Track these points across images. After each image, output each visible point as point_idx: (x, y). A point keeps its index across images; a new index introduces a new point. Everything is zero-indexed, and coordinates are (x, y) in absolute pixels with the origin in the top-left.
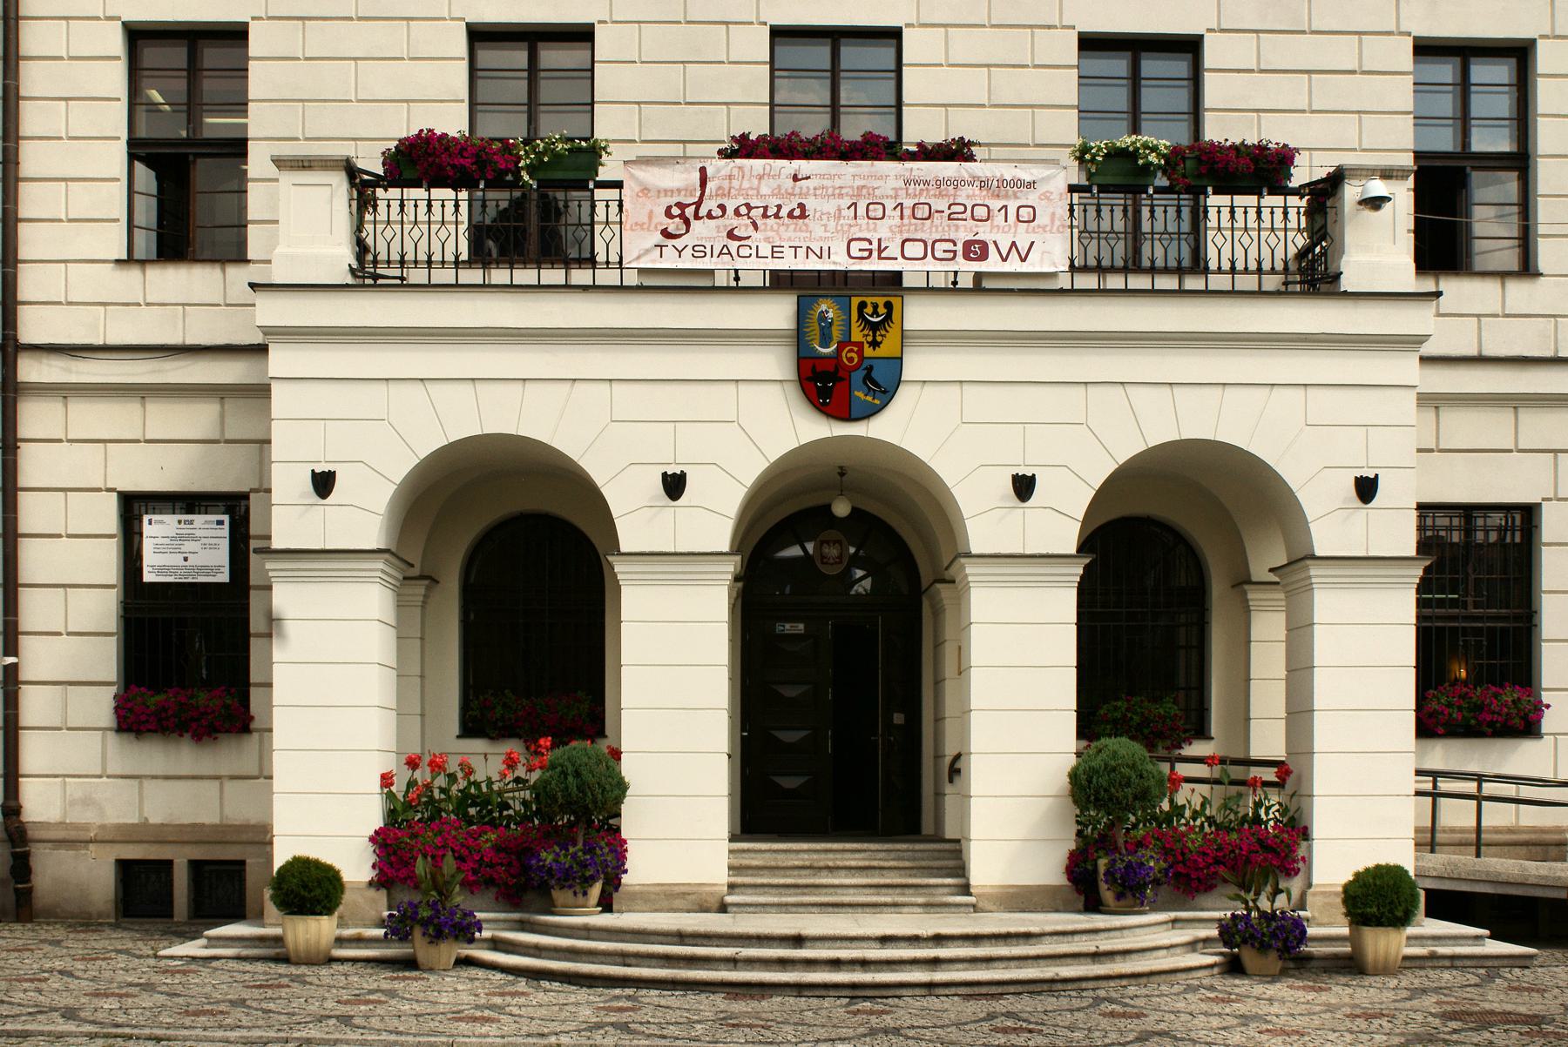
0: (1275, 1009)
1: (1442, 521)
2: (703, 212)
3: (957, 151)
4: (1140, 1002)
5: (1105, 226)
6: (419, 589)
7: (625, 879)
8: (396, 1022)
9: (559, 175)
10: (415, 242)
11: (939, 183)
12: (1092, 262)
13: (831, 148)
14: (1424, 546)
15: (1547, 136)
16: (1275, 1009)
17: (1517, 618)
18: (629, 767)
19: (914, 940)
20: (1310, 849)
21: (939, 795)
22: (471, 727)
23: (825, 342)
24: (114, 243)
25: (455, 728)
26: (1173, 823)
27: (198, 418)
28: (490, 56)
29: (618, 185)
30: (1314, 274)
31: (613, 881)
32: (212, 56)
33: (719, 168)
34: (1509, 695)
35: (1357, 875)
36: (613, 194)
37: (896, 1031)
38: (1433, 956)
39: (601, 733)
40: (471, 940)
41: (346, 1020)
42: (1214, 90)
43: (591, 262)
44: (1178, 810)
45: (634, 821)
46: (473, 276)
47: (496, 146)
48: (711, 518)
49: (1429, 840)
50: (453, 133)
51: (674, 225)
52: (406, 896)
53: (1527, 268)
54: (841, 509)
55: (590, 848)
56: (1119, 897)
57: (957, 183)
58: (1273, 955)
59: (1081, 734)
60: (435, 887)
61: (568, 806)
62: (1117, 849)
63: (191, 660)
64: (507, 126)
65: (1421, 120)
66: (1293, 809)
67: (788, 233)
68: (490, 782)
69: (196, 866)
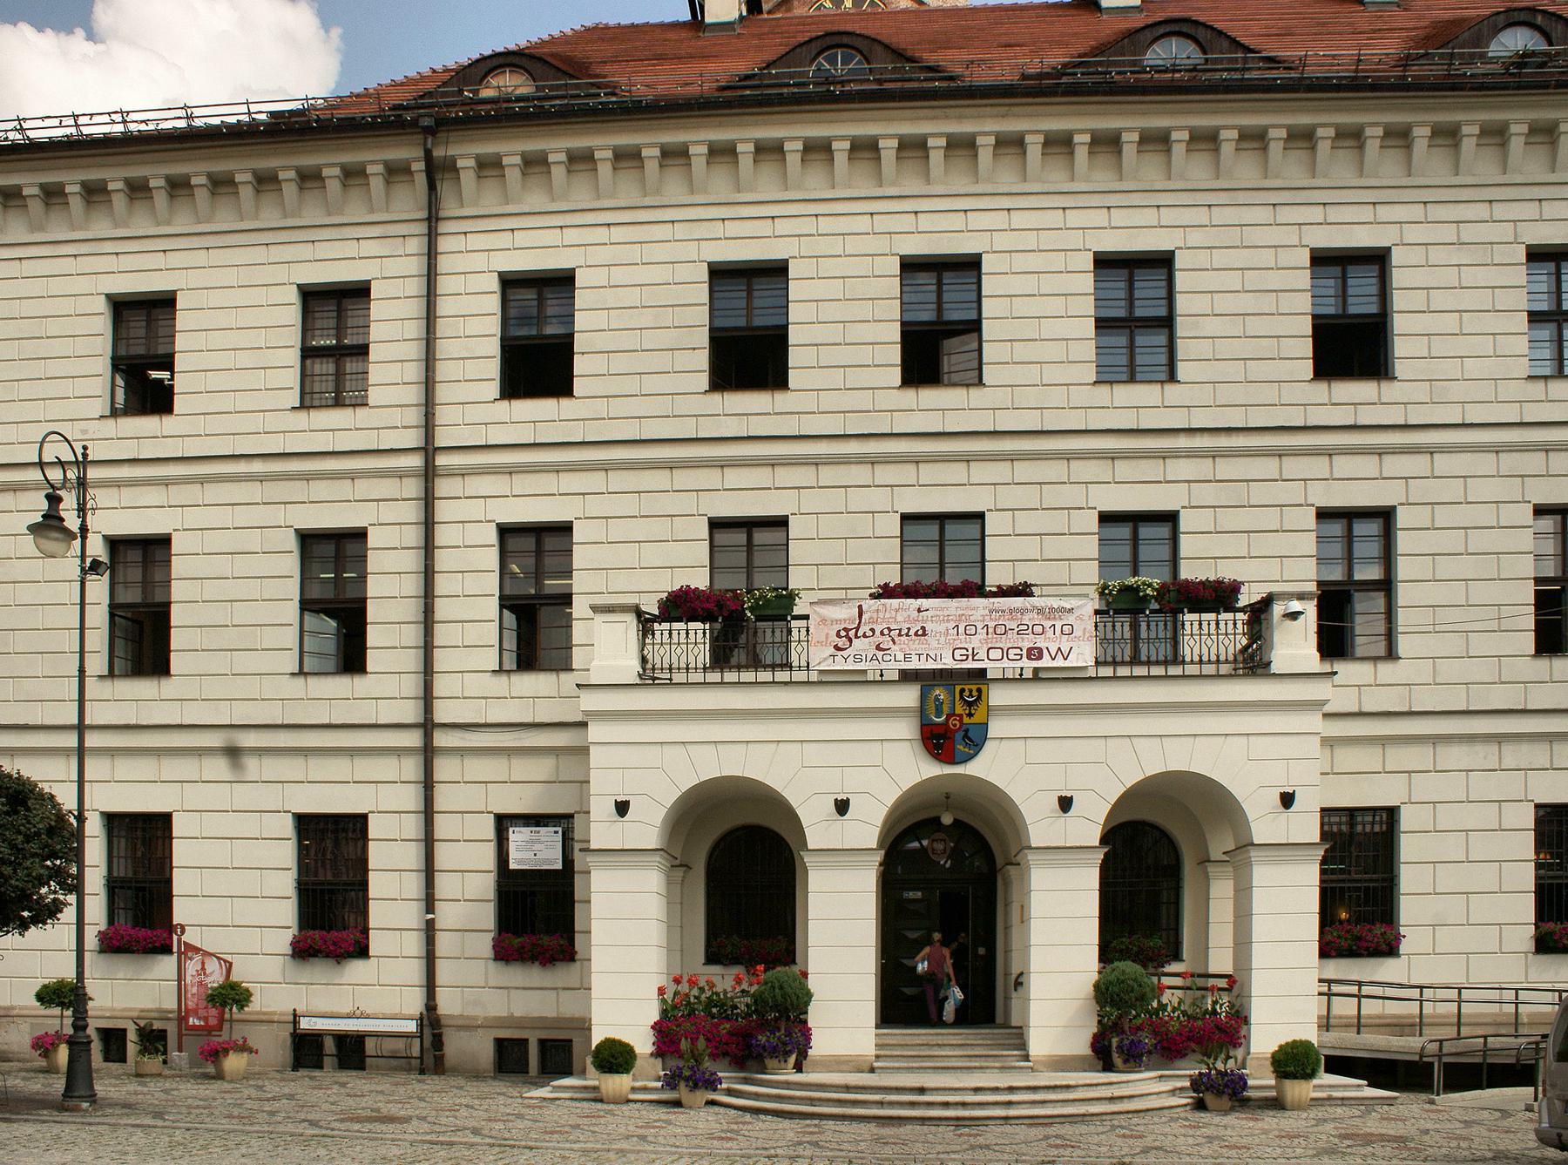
0: (1229, 1132)
1: (1335, 819)
2: (860, 633)
3: (1023, 590)
4: (1141, 1128)
5: (1118, 635)
6: (679, 873)
7: (810, 1052)
8: (673, 1140)
9: (769, 612)
10: (678, 656)
11: (1011, 611)
12: (1110, 659)
13: (942, 591)
14: (1325, 836)
15: (1405, 568)
16: (1229, 1132)
17: (1384, 880)
18: (813, 983)
19: (996, 1090)
20: (1249, 1030)
21: (1007, 999)
22: (712, 958)
23: (939, 713)
24: (491, 659)
25: (701, 958)
26: (1160, 1016)
27: (541, 768)
28: (723, 537)
29: (807, 617)
30: (1253, 662)
31: (803, 1054)
32: (550, 542)
33: (870, 605)
34: (1379, 929)
35: (1281, 1047)
36: (803, 623)
37: (987, 1147)
38: (1330, 1098)
39: (794, 962)
40: (715, 1090)
41: (643, 1138)
42: (1187, 546)
43: (787, 666)
44: (1163, 1007)
45: (816, 1017)
46: (714, 677)
47: (729, 595)
48: (866, 828)
49: (1326, 1024)
50: (702, 588)
51: (842, 642)
52: (674, 1062)
53: (1391, 654)
54: (947, 820)
55: (788, 1034)
56: (1125, 1061)
57: (1023, 611)
58: (1225, 1098)
59: (1101, 960)
60: (693, 1056)
61: (776, 1008)
62: (1125, 1031)
63: (537, 916)
64: (737, 582)
65: (1103, 563)
66: (1238, 1004)
67: (916, 645)
68: (725, 992)
69: (543, 1043)
